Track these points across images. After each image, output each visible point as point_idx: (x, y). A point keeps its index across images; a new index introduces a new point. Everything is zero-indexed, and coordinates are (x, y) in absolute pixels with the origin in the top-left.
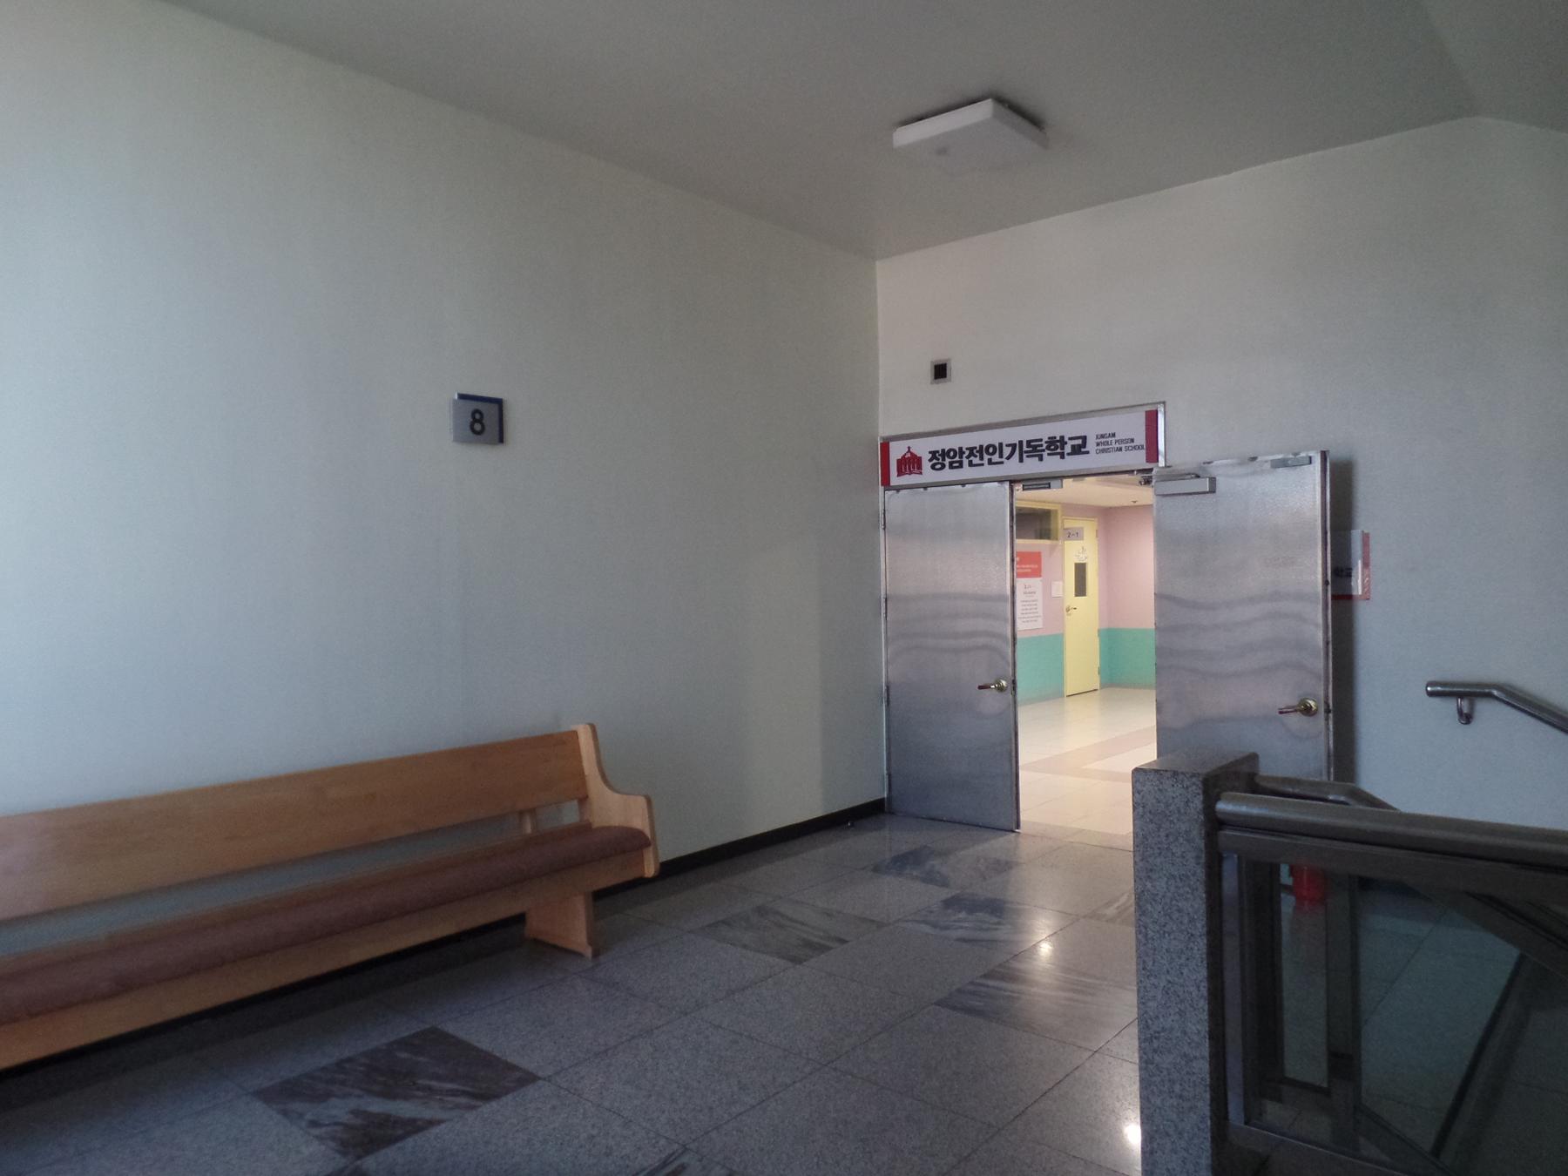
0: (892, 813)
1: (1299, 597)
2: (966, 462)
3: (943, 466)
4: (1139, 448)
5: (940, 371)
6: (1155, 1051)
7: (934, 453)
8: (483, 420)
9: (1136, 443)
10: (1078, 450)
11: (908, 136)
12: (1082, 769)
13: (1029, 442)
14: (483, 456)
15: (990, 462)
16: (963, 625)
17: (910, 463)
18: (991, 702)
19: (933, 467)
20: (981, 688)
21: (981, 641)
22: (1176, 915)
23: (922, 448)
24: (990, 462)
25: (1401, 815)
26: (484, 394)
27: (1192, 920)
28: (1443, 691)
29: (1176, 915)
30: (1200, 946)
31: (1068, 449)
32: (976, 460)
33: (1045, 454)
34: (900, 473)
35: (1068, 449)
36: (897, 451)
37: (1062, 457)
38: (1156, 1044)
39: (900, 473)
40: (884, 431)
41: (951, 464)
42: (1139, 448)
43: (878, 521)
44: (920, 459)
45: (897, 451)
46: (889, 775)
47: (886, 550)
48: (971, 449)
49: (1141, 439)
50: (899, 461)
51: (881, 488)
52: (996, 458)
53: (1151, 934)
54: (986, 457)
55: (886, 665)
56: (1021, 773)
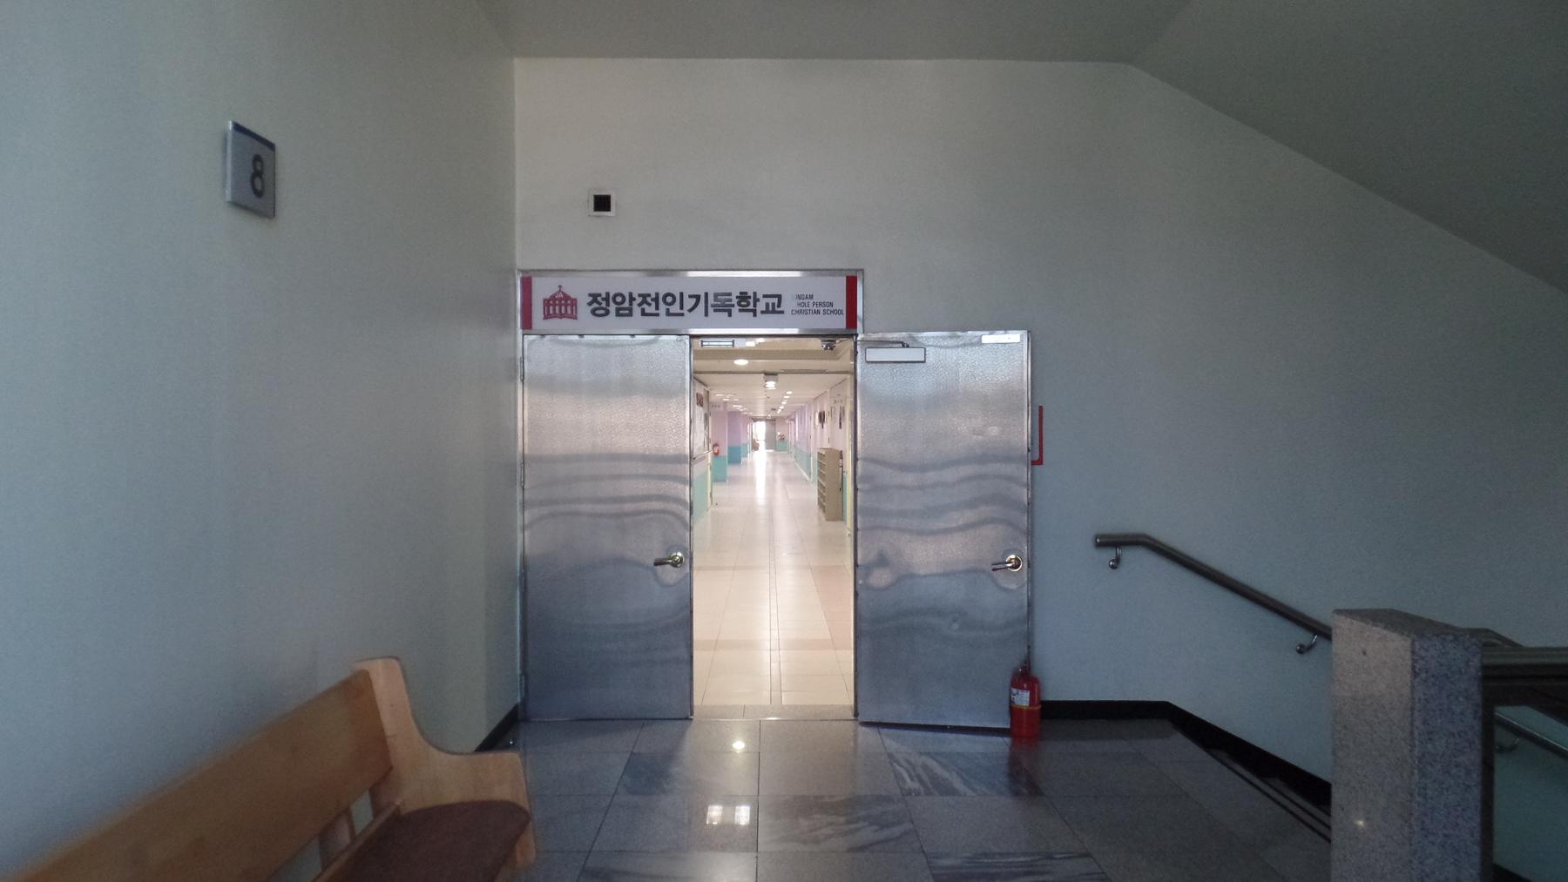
1: (1007, 459)
2: (637, 310)
3: (607, 313)
4: (839, 312)
7: (595, 297)
8: (256, 175)
9: (836, 307)
12: (771, 634)
13: (716, 295)
14: (251, 227)
17: (561, 306)
18: (669, 574)
19: (593, 312)
20: (656, 564)
21: (656, 505)
22: (1454, 771)
23: (579, 289)
24: (668, 314)
25: (1528, 649)
26: (264, 135)
29: (1454, 771)
30: (1476, 793)
31: (761, 306)
33: (735, 310)
34: (547, 316)
35: (761, 306)
36: (543, 289)
39: (547, 316)
41: (618, 310)
42: (839, 312)
43: (513, 370)
44: (574, 303)
45: (543, 289)
46: (525, 673)
47: (525, 405)
48: (644, 296)
49: (841, 304)
52: (675, 308)
53: (1429, 792)
54: (663, 307)
55: (528, 540)
56: (698, 655)
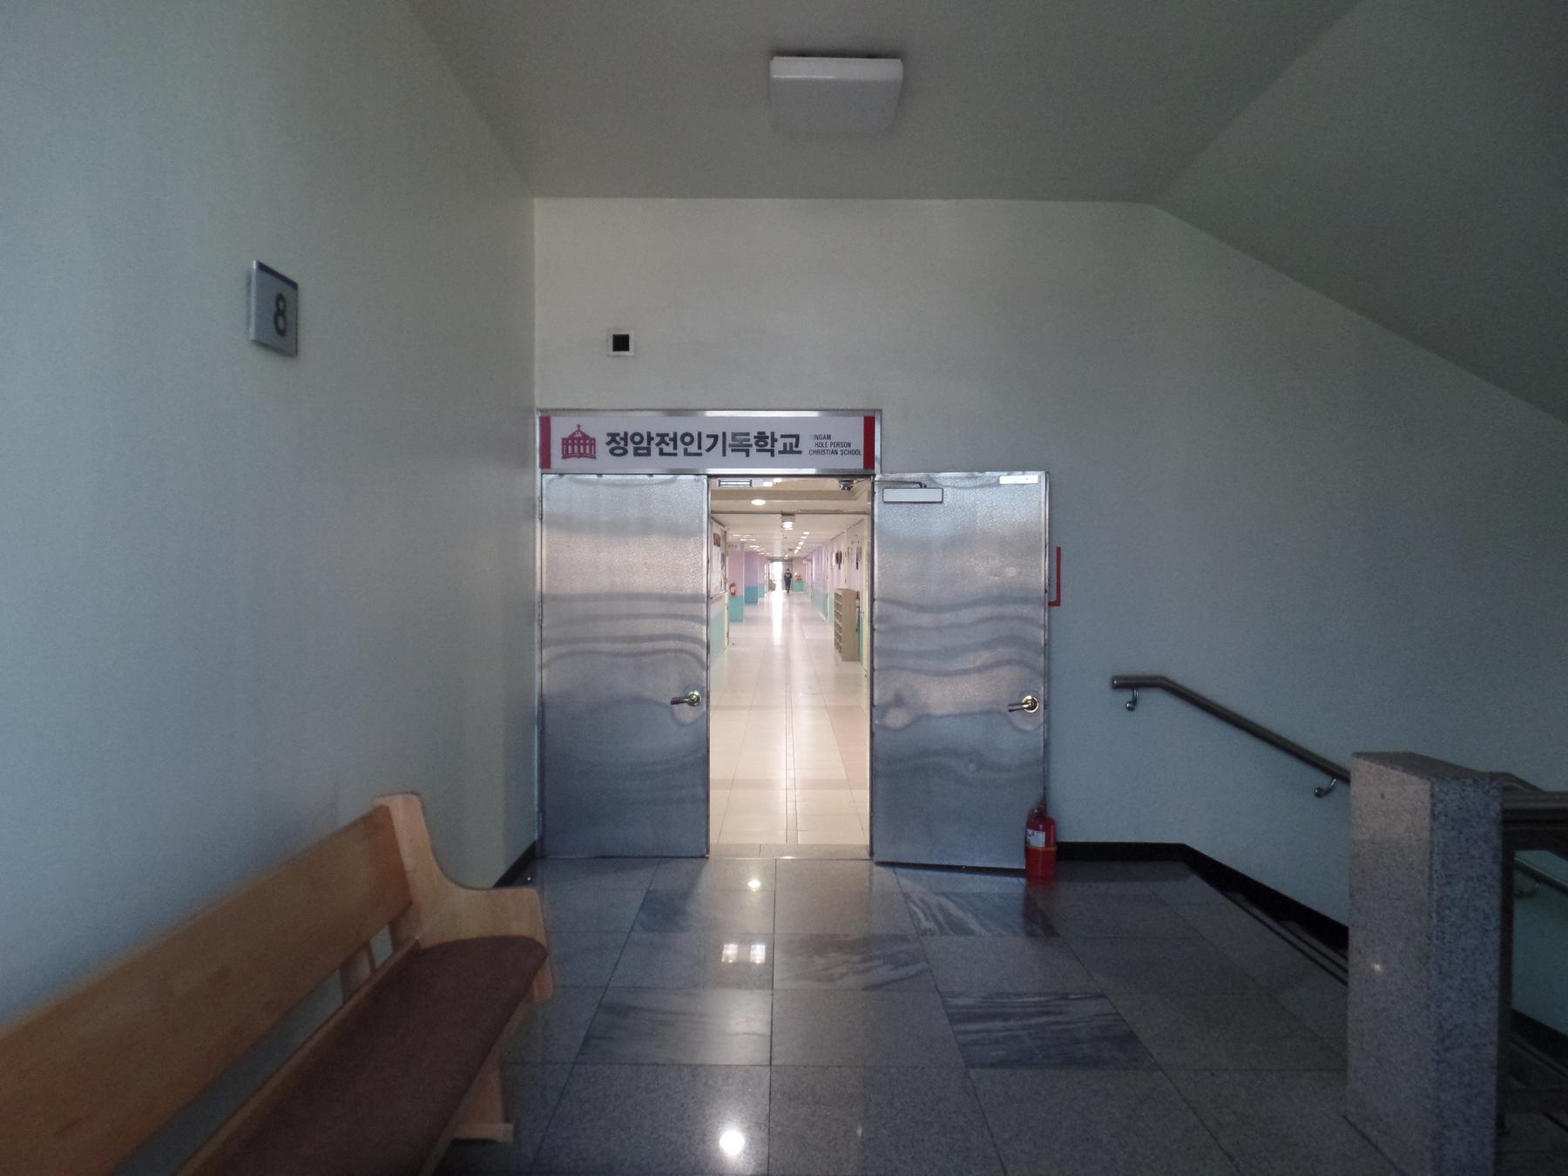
0: (543, 857)
2: (655, 450)
3: (626, 452)
4: (856, 452)
5: (621, 343)
6: (1447, 1050)
8: (279, 315)
10: (791, 450)
11: (789, 70)
12: (787, 772)
13: (734, 435)
15: (686, 453)
16: (646, 627)
17: (580, 445)
18: (686, 713)
21: (672, 644)
23: (598, 429)
27: (1487, 917)
28: (1124, 684)
29: (1472, 915)
31: (779, 446)
32: (669, 449)
33: (753, 450)
34: (566, 456)
35: (779, 446)
36: (562, 428)
37: (772, 452)
38: (1448, 1042)
39: (566, 456)
40: (541, 400)
42: (856, 452)
43: (532, 509)
45: (562, 428)
46: (542, 810)
47: (544, 545)
48: (662, 436)
50: (565, 442)
51: (539, 470)
54: (681, 447)
55: (545, 680)
